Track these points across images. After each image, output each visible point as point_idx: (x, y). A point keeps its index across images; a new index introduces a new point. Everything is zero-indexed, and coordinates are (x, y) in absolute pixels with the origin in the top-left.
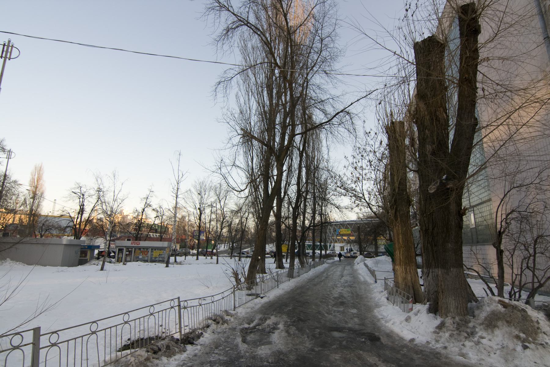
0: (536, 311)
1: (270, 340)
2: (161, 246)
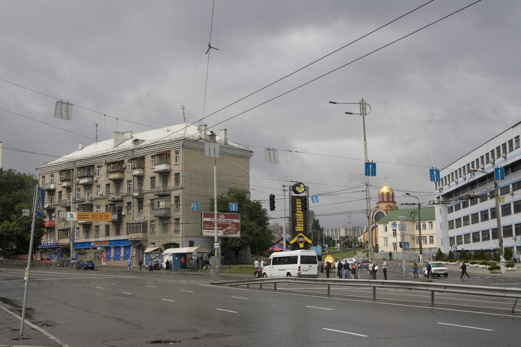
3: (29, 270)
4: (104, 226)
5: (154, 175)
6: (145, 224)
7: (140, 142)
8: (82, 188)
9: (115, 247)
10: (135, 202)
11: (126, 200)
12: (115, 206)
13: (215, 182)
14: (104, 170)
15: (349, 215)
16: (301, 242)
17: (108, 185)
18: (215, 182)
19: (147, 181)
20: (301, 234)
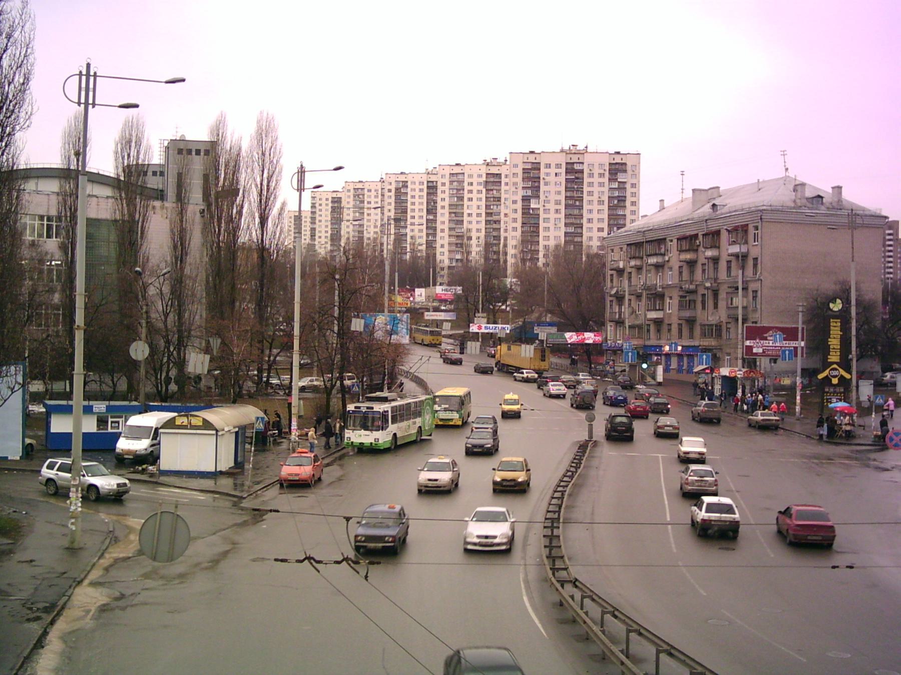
0: (731, 203)
1: (879, 296)
2: (76, 342)
3: (254, 456)
4: (676, 326)
5: (729, 258)
6: (719, 327)
7: (790, 538)
8: (653, 269)
9: (688, 355)
10: (710, 295)
11: (701, 291)
12: (688, 299)
13: (798, 401)
14: (673, 245)
15: (90, 106)
16: (835, 377)
17: (680, 267)
18: (798, 401)
19: (723, 265)
20: (835, 366)
